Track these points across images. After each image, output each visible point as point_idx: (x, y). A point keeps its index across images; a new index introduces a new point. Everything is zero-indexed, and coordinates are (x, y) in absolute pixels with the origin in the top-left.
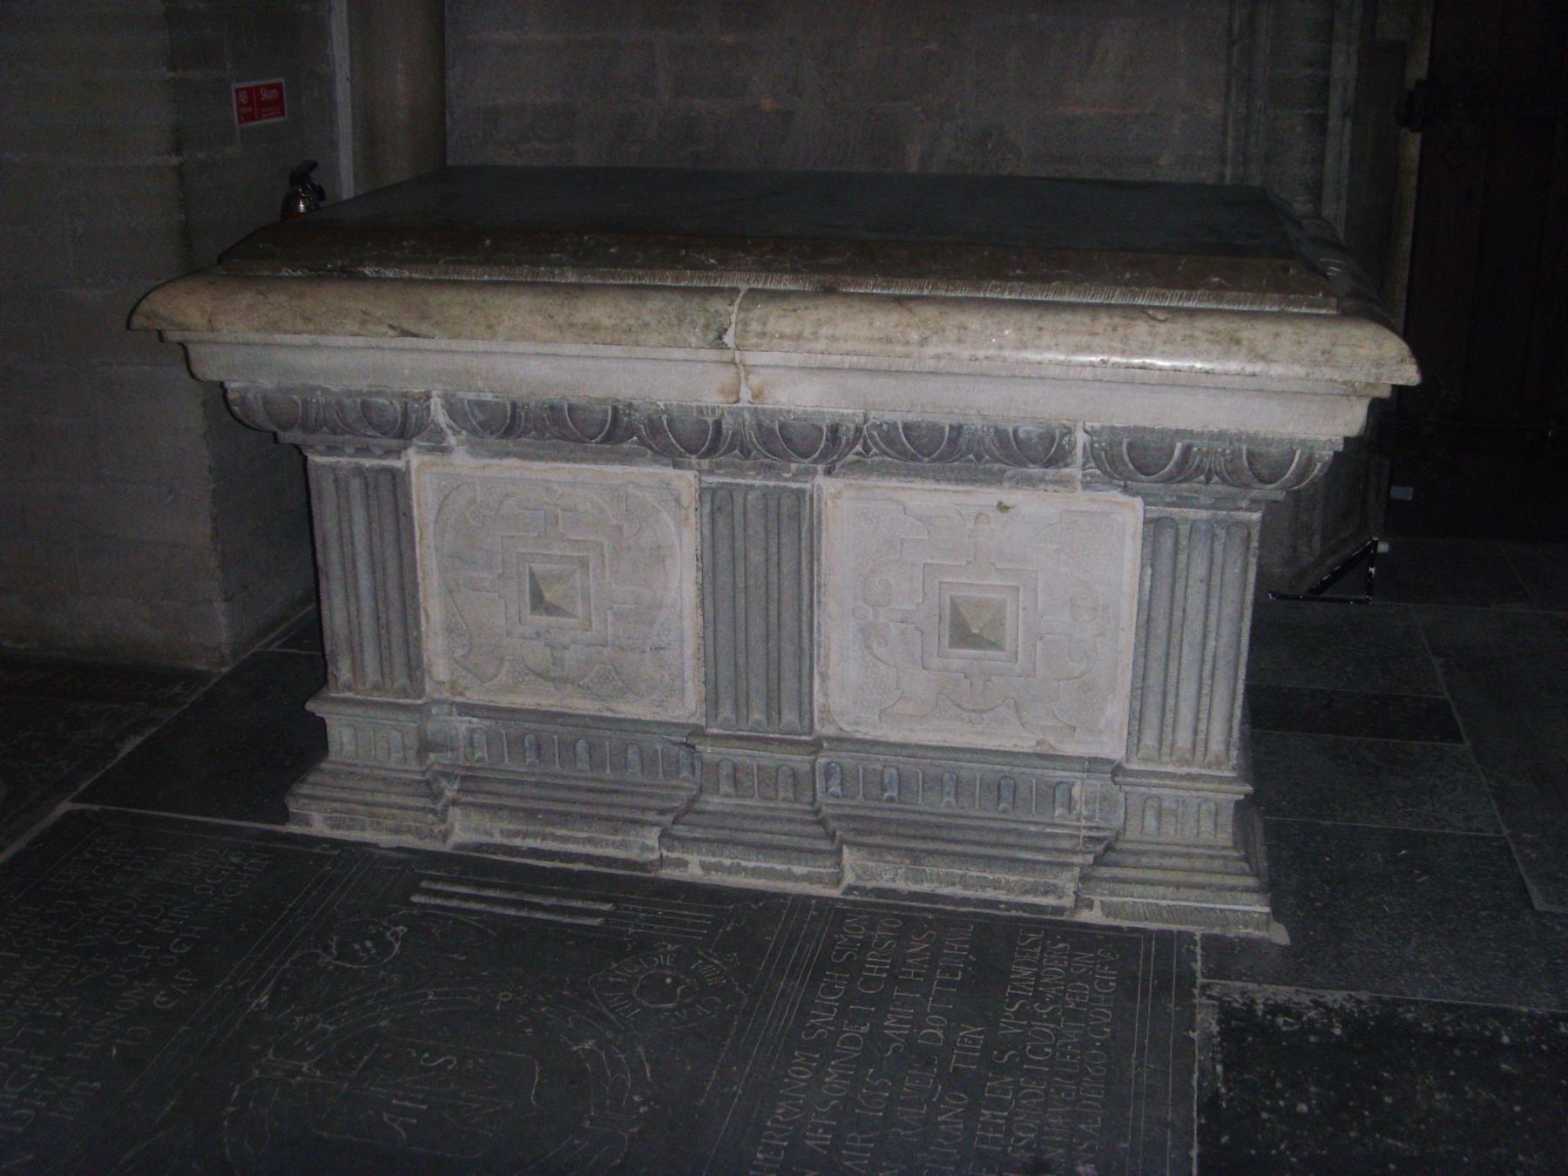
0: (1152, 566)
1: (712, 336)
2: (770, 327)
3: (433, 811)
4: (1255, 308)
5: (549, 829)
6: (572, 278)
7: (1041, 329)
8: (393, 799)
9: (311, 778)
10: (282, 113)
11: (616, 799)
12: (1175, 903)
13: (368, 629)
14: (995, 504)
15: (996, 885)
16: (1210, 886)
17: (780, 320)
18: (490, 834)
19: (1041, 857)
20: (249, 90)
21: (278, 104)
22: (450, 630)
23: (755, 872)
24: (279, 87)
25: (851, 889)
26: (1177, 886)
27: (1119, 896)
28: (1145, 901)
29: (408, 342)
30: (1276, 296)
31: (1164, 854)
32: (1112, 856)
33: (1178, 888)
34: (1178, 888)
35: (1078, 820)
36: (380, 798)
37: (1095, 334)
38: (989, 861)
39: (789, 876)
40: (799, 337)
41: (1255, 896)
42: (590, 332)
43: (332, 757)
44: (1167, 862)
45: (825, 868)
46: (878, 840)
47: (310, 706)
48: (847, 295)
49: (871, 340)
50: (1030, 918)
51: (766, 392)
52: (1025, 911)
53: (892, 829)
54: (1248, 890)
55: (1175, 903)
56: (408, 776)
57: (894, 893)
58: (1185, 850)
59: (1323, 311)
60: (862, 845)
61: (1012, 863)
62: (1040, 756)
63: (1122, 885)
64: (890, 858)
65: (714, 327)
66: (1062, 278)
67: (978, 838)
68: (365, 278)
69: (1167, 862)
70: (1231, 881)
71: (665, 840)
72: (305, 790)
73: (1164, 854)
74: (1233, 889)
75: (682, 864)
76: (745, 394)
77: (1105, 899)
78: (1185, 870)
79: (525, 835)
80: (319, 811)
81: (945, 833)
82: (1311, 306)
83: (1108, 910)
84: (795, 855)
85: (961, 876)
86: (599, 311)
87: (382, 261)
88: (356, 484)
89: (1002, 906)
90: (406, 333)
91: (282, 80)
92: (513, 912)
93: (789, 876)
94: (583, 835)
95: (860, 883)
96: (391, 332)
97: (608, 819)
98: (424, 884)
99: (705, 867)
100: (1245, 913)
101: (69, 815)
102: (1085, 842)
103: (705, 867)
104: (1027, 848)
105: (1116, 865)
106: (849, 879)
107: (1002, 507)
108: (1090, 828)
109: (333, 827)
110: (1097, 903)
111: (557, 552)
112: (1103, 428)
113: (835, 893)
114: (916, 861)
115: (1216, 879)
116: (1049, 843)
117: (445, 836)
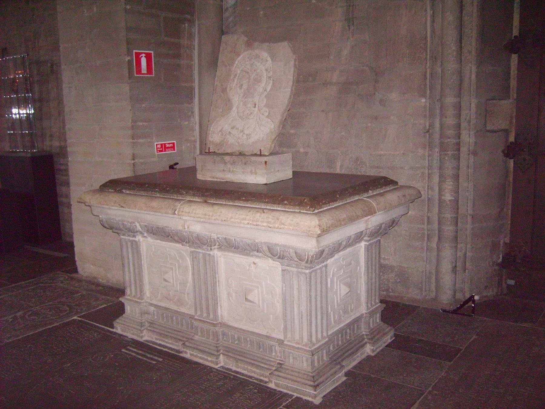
0: (285, 283)
1: (173, 211)
2: (185, 210)
3: (140, 330)
4: (294, 211)
5: (164, 339)
6: (158, 195)
7: (237, 213)
8: (134, 326)
9: (120, 318)
10: (174, 150)
11: (179, 333)
12: (292, 386)
13: (133, 281)
14: (253, 262)
15: (254, 372)
16: (301, 382)
17: (187, 208)
18: (153, 339)
19: (266, 366)
20: (162, 144)
21: (173, 148)
22: (150, 283)
23: (201, 358)
24: (174, 144)
25: (222, 367)
26: (292, 380)
27: (278, 381)
28: (285, 383)
29: (122, 209)
30: (298, 207)
31: (292, 371)
32: (280, 369)
33: (292, 381)
34: (292, 381)
35: (278, 357)
36: (131, 325)
37: (248, 215)
38: (253, 364)
39: (207, 360)
40: (189, 212)
41: (311, 388)
42: (152, 209)
43: (126, 314)
44: (293, 373)
45: (214, 359)
46: (230, 354)
47: (121, 299)
48: (208, 202)
49: (202, 214)
50: (257, 383)
51: (190, 227)
52: (258, 381)
53: (234, 352)
54: (311, 386)
55: (292, 386)
56: (138, 320)
57: (230, 370)
58: (299, 371)
59: (309, 212)
60: (226, 355)
61: (258, 367)
62: (267, 336)
63: (279, 377)
64: (231, 360)
65: (174, 209)
66: (252, 200)
67: (253, 358)
68: (123, 192)
69: (293, 373)
70: (307, 382)
71: (183, 345)
72: (118, 321)
73: (292, 371)
74: (306, 384)
75: (186, 353)
76: (186, 227)
77: (276, 381)
78: (296, 377)
79: (160, 340)
80: (119, 326)
81: (245, 355)
82: (306, 210)
83: (277, 385)
84: (208, 354)
85: (247, 368)
86: (155, 204)
87: (126, 189)
88: (129, 244)
89: (253, 378)
90: (122, 207)
91: (175, 142)
92: (140, 357)
93: (207, 360)
94: (170, 342)
95: (225, 366)
96: (119, 206)
97: (175, 338)
98: (129, 347)
99: (191, 355)
100: (309, 392)
101: (75, 320)
102: (277, 364)
103: (191, 355)
104: (263, 363)
105: (280, 372)
106: (222, 364)
107: (254, 263)
108: (280, 360)
109: (122, 331)
110: (273, 382)
111: (168, 266)
112: (259, 242)
113: (216, 367)
114: (237, 362)
115: (304, 381)
116: (268, 363)
117: (142, 337)
